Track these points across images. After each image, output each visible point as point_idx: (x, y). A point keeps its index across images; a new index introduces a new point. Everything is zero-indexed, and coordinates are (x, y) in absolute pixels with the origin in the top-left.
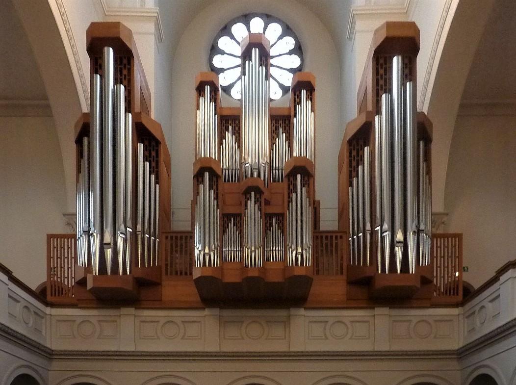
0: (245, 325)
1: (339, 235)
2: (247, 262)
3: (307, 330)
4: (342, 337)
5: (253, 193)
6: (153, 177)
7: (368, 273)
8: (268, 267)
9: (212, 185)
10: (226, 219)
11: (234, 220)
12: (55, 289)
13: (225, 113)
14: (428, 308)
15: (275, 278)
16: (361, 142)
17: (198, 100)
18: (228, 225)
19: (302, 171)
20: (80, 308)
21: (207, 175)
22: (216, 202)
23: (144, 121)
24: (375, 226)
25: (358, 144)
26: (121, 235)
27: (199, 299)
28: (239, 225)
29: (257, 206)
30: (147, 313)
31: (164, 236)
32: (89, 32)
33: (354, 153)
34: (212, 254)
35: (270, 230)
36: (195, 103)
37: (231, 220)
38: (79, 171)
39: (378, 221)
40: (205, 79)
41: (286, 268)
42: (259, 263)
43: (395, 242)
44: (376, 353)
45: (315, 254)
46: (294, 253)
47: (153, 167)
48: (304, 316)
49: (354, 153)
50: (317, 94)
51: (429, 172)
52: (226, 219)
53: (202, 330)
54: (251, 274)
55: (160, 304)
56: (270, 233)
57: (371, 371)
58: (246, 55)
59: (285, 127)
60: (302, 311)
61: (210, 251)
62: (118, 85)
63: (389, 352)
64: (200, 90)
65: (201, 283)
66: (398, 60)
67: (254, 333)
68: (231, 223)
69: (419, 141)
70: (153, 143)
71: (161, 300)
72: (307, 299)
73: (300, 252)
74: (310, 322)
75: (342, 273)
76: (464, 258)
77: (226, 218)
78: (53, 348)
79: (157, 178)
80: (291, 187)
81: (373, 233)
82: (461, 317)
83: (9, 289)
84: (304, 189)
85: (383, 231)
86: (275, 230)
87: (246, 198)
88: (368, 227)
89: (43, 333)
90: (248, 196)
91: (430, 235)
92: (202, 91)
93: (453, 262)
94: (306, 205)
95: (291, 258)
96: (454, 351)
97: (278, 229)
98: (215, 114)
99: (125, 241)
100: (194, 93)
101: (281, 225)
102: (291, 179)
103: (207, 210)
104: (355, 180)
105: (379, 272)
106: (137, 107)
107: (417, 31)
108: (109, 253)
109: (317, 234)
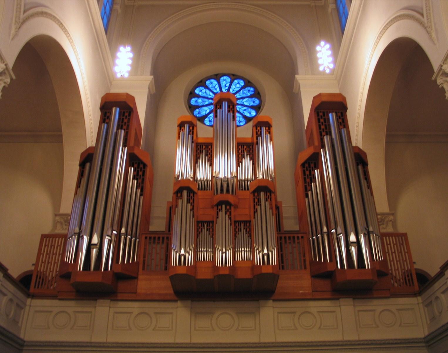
0: (216, 315)
1: (300, 235)
2: (218, 262)
3: (272, 323)
4: (310, 327)
5: (224, 206)
6: (139, 191)
7: (330, 268)
8: (237, 265)
9: (189, 199)
10: (200, 225)
11: (207, 226)
12: (39, 282)
13: (200, 141)
14: (388, 298)
15: (244, 274)
16: (312, 165)
17: (179, 134)
18: (202, 231)
19: (263, 190)
20: (60, 299)
21: (185, 193)
22: (192, 212)
23: (136, 152)
24: (330, 228)
25: (310, 167)
26: (107, 237)
27: (172, 291)
28: (211, 230)
29: (227, 216)
30: (121, 304)
31: (143, 238)
32: (103, 98)
33: (307, 173)
34: (187, 255)
35: (239, 234)
36: (176, 136)
37: (204, 226)
38: (78, 185)
39: (333, 225)
40: (185, 120)
41: (254, 267)
42: (230, 263)
43: (349, 243)
44: (346, 343)
45: (279, 240)
46: (261, 254)
47: (140, 183)
48: (273, 307)
49: (307, 173)
50: (274, 130)
51: (369, 187)
52: (200, 225)
53: (178, 323)
54: (221, 272)
55: (135, 297)
56: (239, 236)
57: (124, 308)
58: (218, 105)
59: (249, 150)
60: (270, 303)
61: (185, 252)
62: (120, 130)
63: (358, 341)
64: (181, 126)
65: (175, 279)
66: (310, 192)
67: (225, 325)
68: (204, 228)
69: (358, 164)
70: (141, 166)
71: (136, 293)
72: (274, 292)
73: (266, 254)
74: (279, 313)
75: (305, 268)
76: (412, 252)
77: (200, 224)
78: (26, 339)
79: (142, 191)
80: (256, 200)
81: (329, 234)
82: (421, 305)
83: (2, 285)
84: (267, 203)
85: (338, 233)
86: (243, 234)
87: (217, 209)
88: (325, 229)
89: (20, 325)
90: (220, 207)
91: (379, 235)
92: (183, 127)
93: (404, 257)
94: (270, 215)
95: (258, 257)
96: (420, 339)
97: (246, 233)
98: (192, 142)
99: (110, 242)
100: (176, 129)
101: (248, 230)
102: (256, 194)
103: (201, 243)
104: (309, 193)
105: (339, 267)
106: (132, 143)
107: (344, 99)
108: (94, 251)
109: (281, 235)
